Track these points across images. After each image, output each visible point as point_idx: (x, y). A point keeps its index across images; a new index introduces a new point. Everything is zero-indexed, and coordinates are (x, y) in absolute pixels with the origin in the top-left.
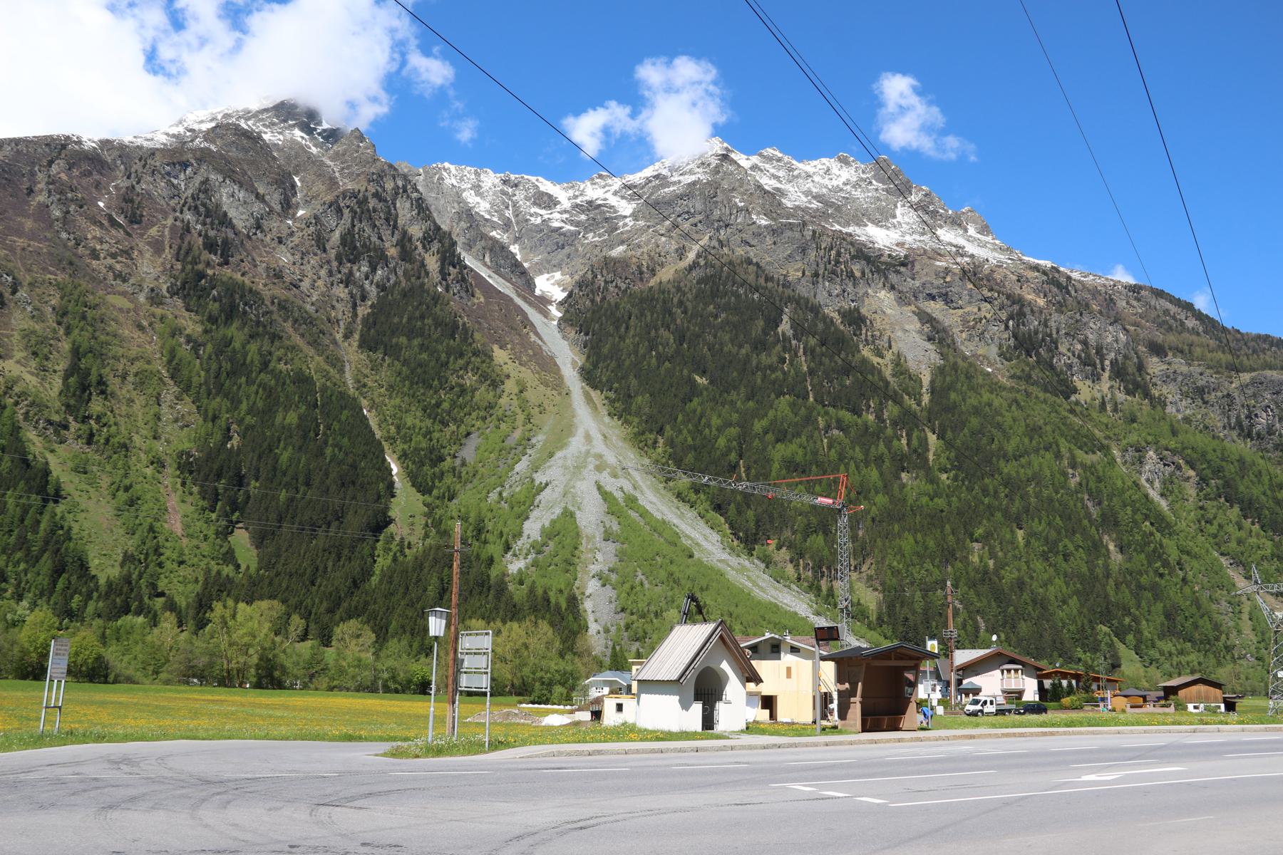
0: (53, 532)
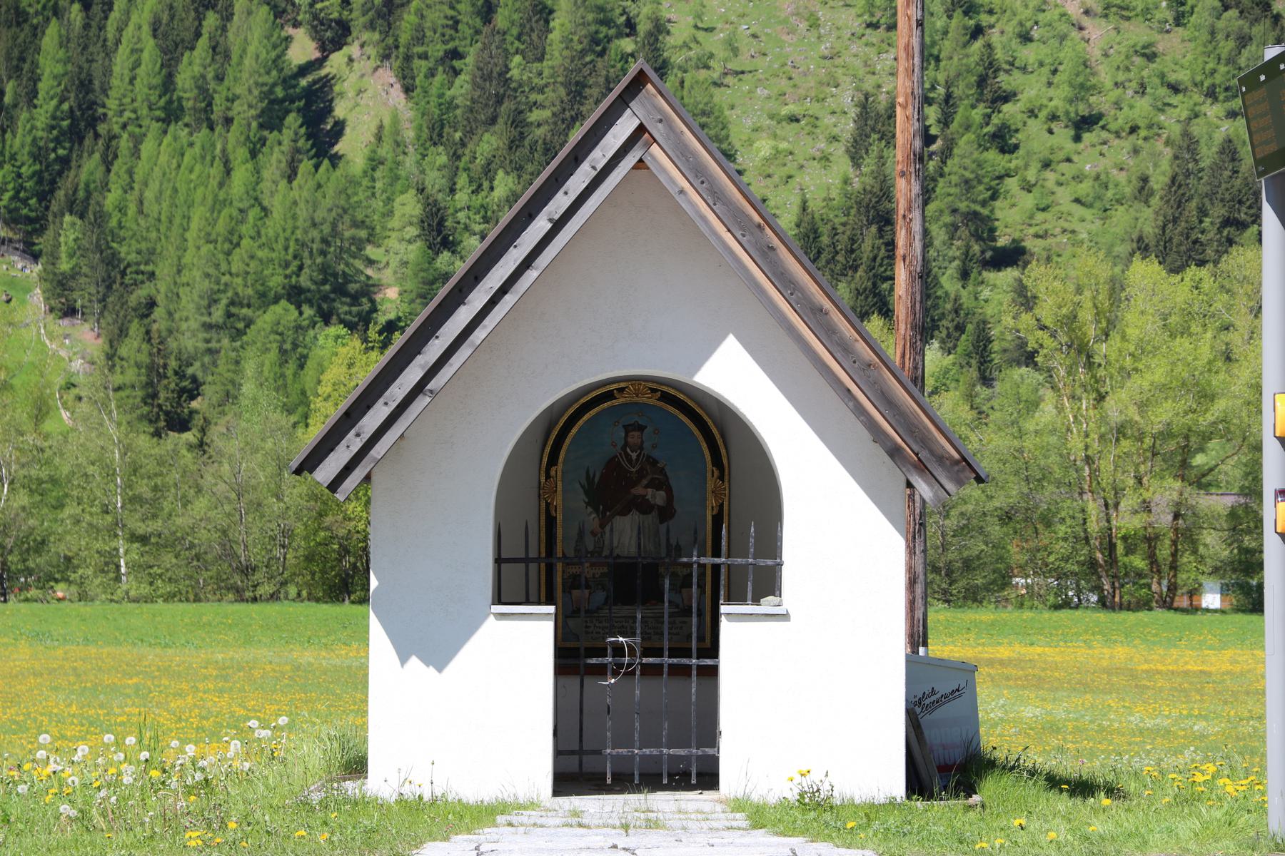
0: (598, 45)
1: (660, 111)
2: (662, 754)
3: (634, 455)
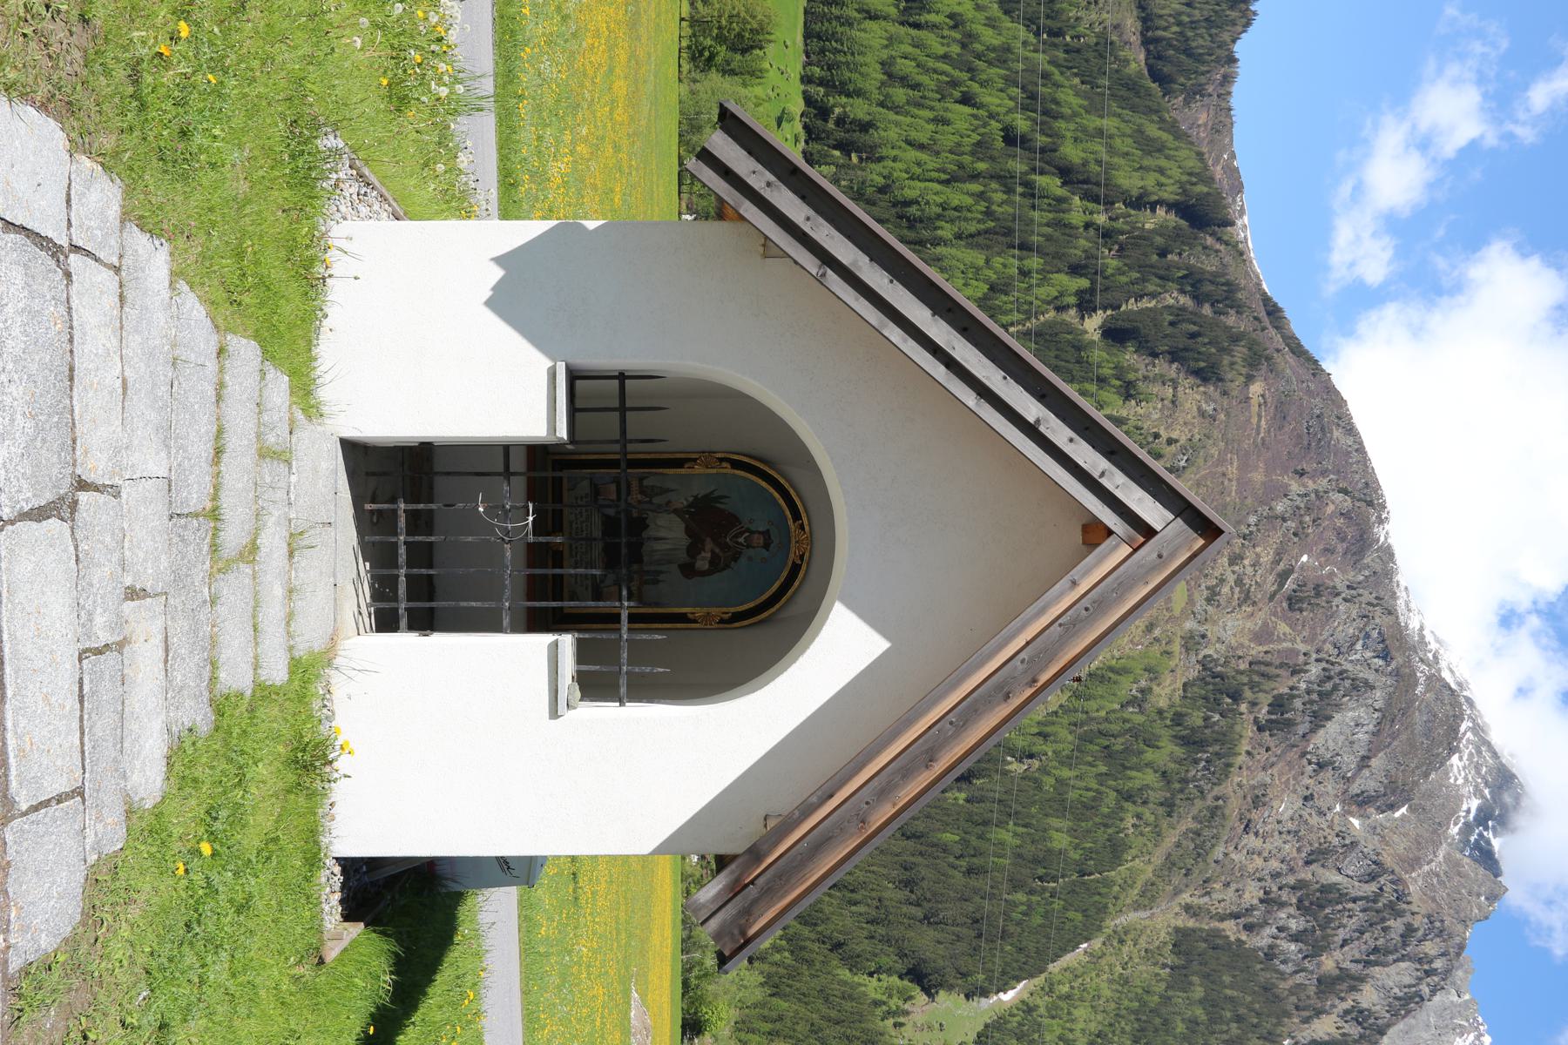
1: (1173, 555)
2: (397, 567)
3: (741, 540)
